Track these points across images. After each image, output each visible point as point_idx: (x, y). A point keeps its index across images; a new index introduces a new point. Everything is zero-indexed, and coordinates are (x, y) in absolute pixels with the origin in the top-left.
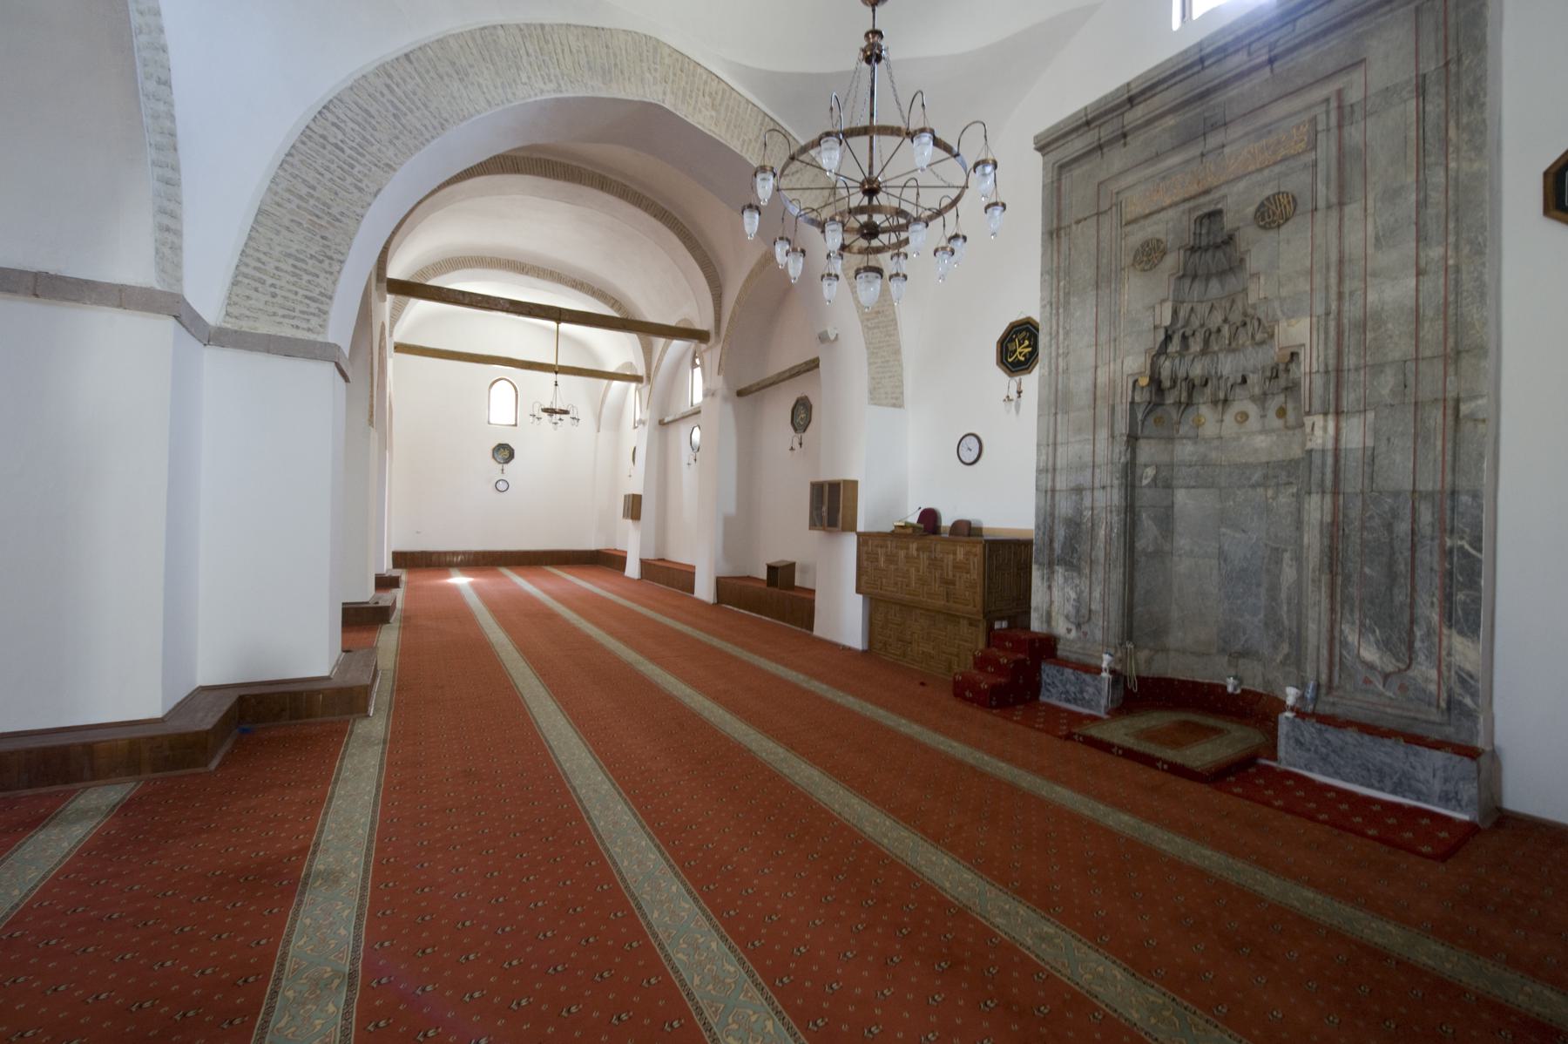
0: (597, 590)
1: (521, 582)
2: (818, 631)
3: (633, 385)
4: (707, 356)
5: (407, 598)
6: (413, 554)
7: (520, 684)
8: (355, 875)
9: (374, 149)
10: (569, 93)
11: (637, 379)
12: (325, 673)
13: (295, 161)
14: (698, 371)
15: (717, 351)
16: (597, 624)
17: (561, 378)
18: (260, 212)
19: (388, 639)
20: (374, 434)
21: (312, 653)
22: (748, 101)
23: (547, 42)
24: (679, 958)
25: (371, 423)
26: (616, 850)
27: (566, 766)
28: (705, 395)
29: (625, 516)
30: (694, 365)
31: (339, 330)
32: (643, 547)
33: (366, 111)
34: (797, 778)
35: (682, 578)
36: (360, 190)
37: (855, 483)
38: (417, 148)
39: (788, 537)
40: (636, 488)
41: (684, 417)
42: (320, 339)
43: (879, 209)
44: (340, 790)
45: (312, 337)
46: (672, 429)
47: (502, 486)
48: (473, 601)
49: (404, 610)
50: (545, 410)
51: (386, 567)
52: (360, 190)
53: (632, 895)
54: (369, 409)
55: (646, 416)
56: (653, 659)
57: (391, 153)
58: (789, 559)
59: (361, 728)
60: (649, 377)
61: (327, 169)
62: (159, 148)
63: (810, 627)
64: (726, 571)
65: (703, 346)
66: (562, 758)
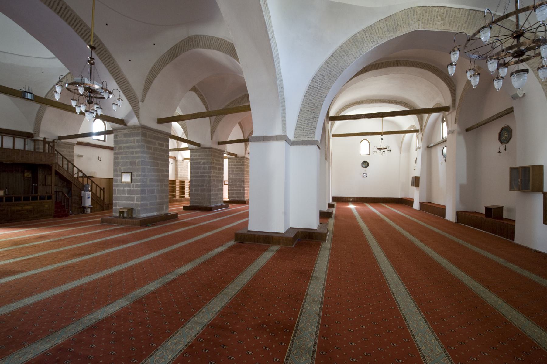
0: (400, 213)
1: (371, 208)
2: (517, 241)
3: (415, 134)
4: (449, 117)
5: (336, 210)
6: (338, 197)
7: (369, 240)
8: (323, 280)
9: (324, 85)
10: (381, 42)
11: (416, 131)
12: (316, 228)
13: (307, 95)
14: (445, 124)
15: (454, 114)
16: (400, 226)
17: (384, 136)
18: (301, 110)
19: (331, 222)
20: (327, 162)
21: (311, 222)
22: (460, 9)
23: (373, 30)
24: (418, 339)
25: (326, 159)
26: (398, 299)
27: (383, 269)
28: (448, 133)
29: (412, 185)
30: (443, 121)
31: (317, 137)
32: (421, 197)
33: (323, 75)
34: (488, 300)
35: (440, 211)
36: (322, 97)
37: (541, 167)
38: (336, 80)
39: (498, 193)
40: (417, 174)
41: (439, 144)
42: (314, 139)
43: (522, 44)
44: (319, 259)
45: (312, 139)
46: (433, 150)
47: (365, 175)
48: (356, 213)
49: (335, 214)
50: (378, 149)
51: (331, 201)
52: (322, 97)
53: (403, 314)
54: (325, 155)
55: (421, 145)
56: (422, 241)
57: (329, 84)
58: (498, 204)
59: (324, 244)
60: (421, 130)
61: (314, 94)
62: (282, 103)
63: (513, 239)
64: (461, 209)
65: (447, 113)
66: (382, 266)
